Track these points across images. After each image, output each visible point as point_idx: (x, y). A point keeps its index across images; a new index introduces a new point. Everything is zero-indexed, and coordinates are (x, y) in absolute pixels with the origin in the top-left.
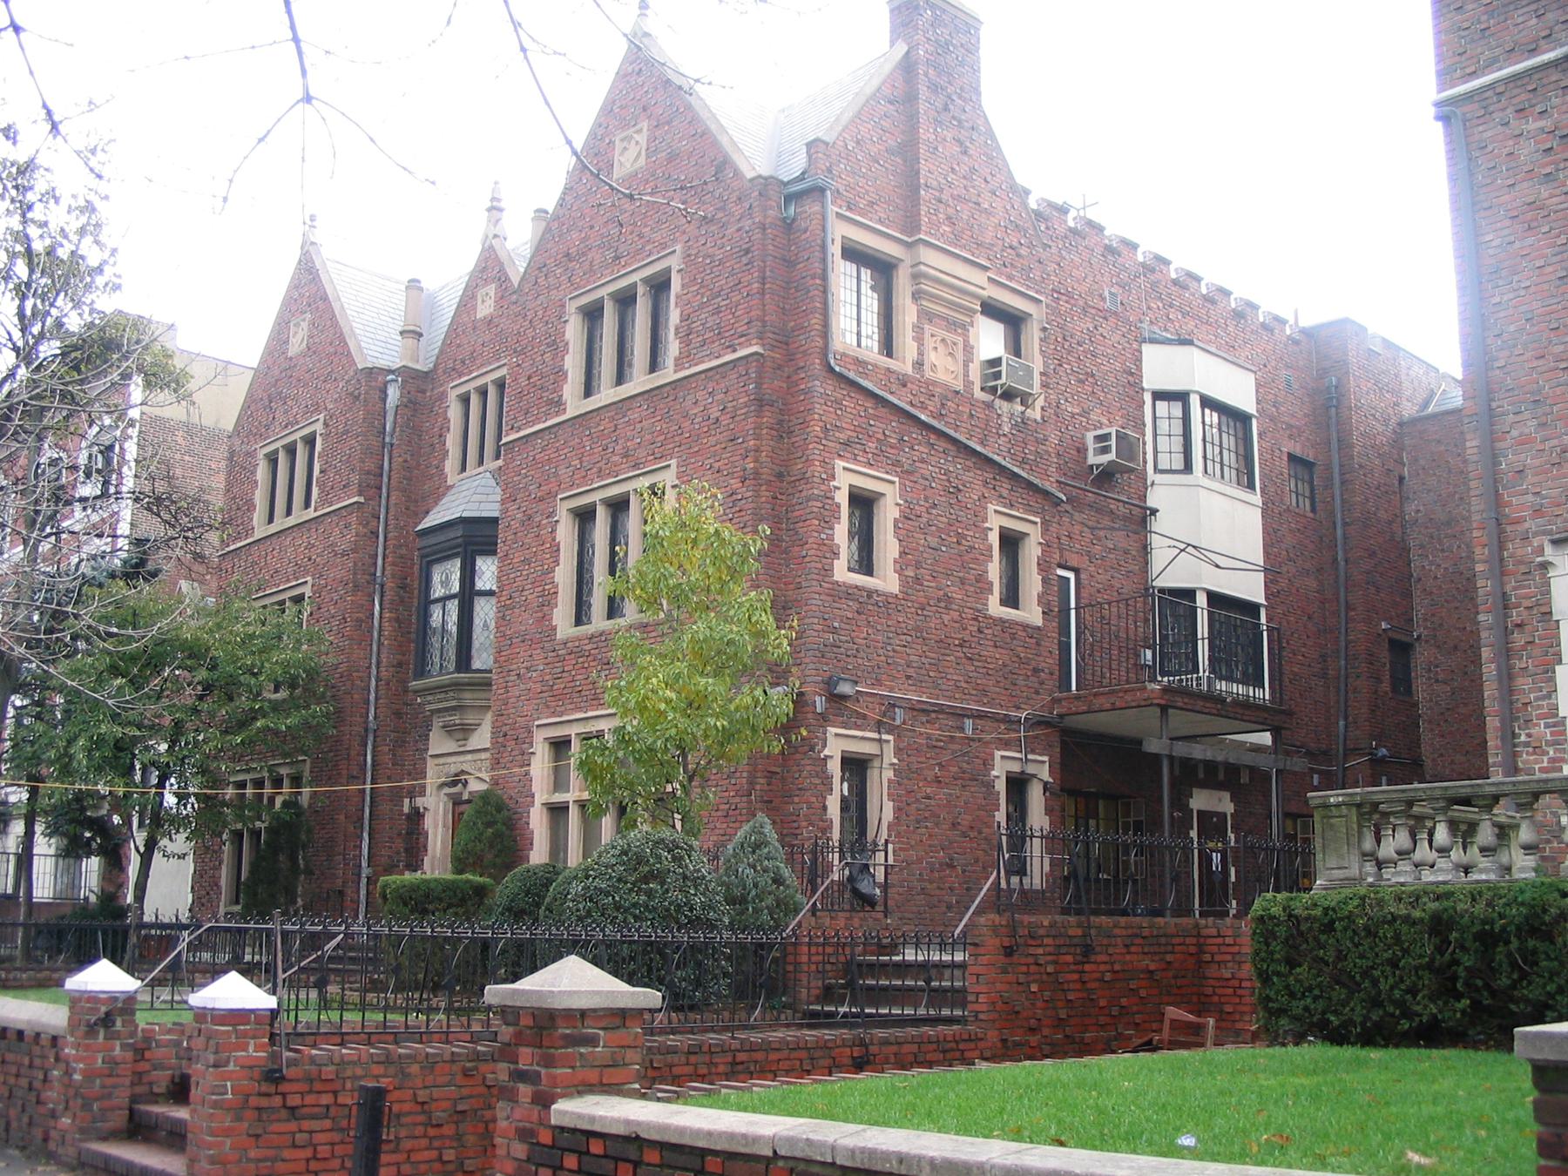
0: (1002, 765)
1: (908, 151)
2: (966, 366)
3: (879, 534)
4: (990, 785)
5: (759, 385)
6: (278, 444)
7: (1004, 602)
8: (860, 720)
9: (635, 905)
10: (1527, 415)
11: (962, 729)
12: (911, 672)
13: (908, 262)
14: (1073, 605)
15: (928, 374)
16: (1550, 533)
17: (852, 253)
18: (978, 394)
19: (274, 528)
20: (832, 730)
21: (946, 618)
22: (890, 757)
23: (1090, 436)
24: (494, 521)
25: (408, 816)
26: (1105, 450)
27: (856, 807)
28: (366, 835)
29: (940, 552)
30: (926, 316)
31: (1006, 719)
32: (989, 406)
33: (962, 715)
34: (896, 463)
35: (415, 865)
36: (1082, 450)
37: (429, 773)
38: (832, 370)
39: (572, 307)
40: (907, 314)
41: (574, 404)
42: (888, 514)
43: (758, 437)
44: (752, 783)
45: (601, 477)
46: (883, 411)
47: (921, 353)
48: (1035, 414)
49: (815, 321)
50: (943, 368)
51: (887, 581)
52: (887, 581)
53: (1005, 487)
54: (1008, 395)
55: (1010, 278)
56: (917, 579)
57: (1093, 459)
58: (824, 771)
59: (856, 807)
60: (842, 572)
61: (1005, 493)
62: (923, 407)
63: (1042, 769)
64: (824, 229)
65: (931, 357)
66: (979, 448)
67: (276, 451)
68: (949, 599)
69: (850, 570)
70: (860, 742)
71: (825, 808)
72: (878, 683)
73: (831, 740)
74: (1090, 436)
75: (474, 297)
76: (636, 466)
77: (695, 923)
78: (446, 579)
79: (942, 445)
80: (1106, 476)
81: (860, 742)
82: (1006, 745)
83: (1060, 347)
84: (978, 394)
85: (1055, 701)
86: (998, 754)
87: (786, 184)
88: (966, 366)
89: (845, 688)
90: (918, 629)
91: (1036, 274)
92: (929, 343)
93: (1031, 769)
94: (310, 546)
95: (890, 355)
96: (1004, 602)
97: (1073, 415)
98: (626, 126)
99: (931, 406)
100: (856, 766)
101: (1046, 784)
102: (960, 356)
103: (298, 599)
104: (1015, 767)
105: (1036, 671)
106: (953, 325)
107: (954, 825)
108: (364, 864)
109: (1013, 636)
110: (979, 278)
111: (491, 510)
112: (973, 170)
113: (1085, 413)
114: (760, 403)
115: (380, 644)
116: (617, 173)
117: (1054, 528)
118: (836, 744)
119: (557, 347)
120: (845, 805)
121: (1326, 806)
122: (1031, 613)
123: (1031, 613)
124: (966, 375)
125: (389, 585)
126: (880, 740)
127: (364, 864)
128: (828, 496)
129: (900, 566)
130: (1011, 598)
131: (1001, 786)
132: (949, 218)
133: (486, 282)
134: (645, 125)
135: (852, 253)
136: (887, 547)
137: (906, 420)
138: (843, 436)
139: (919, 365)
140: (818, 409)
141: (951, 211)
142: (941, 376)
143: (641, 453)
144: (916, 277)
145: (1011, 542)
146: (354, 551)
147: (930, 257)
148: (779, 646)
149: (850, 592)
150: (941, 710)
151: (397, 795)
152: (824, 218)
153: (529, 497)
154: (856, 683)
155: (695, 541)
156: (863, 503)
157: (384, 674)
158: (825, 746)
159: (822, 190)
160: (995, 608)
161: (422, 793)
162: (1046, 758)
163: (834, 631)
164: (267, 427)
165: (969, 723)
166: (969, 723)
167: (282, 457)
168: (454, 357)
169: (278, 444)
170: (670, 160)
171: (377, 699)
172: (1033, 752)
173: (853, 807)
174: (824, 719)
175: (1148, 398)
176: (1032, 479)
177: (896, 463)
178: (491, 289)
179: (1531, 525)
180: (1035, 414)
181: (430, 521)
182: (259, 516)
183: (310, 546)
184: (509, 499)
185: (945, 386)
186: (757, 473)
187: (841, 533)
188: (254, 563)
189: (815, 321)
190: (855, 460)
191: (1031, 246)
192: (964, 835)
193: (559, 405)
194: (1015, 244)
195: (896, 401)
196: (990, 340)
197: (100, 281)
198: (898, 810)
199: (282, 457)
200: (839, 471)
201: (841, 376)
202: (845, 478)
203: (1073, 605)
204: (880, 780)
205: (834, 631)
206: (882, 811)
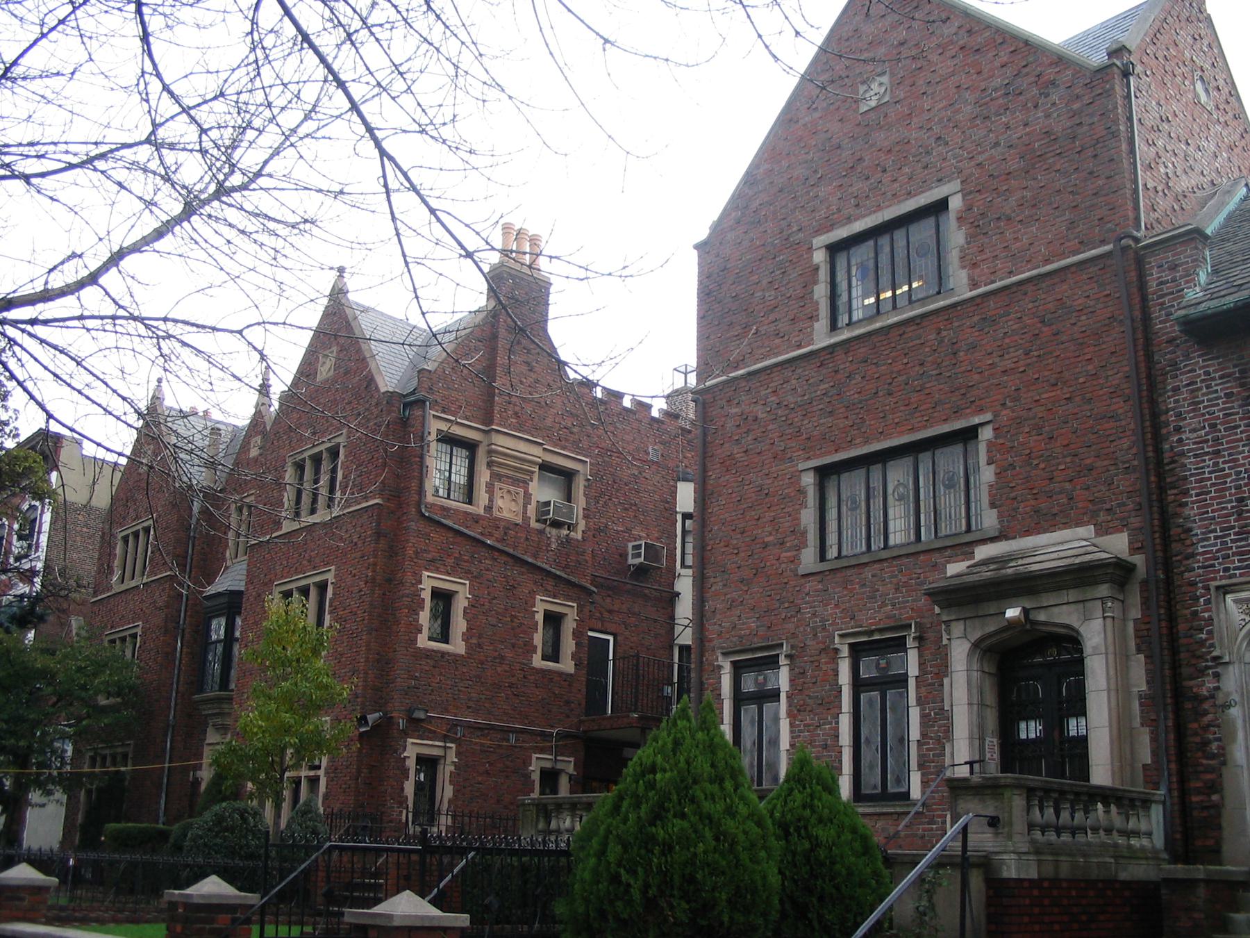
0: (537, 763)
1: (490, 369)
2: (525, 507)
3: (446, 616)
4: (527, 776)
5: (378, 524)
6: (129, 531)
7: (545, 657)
8: (433, 735)
9: (216, 845)
10: (719, 579)
11: (508, 740)
12: (471, 704)
13: (485, 443)
14: (611, 657)
15: (496, 513)
16: (722, 648)
17: (449, 440)
18: (534, 524)
19: (123, 587)
20: (410, 740)
21: (499, 669)
22: (452, 757)
23: (630, 545)
24: (241, 593)
25: (192, 783)
26: (639, 555)
27: (427, 790)
28: (163, 795)
29: (499, 628)
30: (495, 476)
31: (542, 734)
32: (542, 532)
33: (507, 731)
34: (469, 572)
35: (556, 793)
36: (624, 556)
37: (205, 755)
38: (423, 515)
39: (289, 462)
40: (483, 476)
41: (287, 527)
42: (460, 603)
43: (375, 556)
44: (359, 771)
45: (297, 573)
46: (459, 539)
47: (491, 500)
48: (578, 535)
49: (414, 484)
50: (507, 508)
51: (457, 646)
52: (457, 646)
53: (550, 585)
54: (556, 524)
55: (564, 448)
56: (479, 645)
57: (631, 561)
58: (404, 766)
59: (427, 790)
60: (423, 641)
61: (550, 588)
62: (491, 535)
63: (568, 765)
64: (423, 426)
65: (500, 502)
66: (530, 560)
67: (127, 536)
68: (502, 658)
69: (430, 639)
70: (431, 747)
71: (402, 789)
72: (446, 711)
73: (409, 747)
74: (630, 545)
75: (249, 443)
76: (314, 568)
77: (251, 856)
78: (218, 628)
79: (504, 558)
80: (641, 571)
81: (431, 747)
82: (542, 751)
83: (601, 491)
84: (534, 524)
85: (581, 722)
86: (535, 756)
87: (405, 396)
88: (525, 507)
89: (420, 715)
90: (479, 677)
91: (585, 443)
92: (498, 494)
93: (559, 766)
94: (142, 601)
95: (470, 503)
96: (545, 657)
97: (618, 532)
98: (325, 349)
99: (497, 534)
100: (428, 764)
101: (571, 776)
102: (521, 501)
103: (134, 636)
104: (548, 765)
105: (568, 703)
106: (516, 482)
107: (498, 802)
108: (161, 815)
109: (551, 680)
110: (536, 451)
111: (241, 586)
112: (537, 381)
113: (628, 530)
114: (379, 535)
115: (179, 669)
116: (319, 378)
117: (586, 610)
118: (412, 749)
119: (280, 485)
120: (419, 786)
121: (524, 805)
122: (567, 665)
123: (567, 665)
124: (525, 512)
125: (187, 631)
126: (445, 747)
127: (161, 815)
128: (417, 594)
129: (466, 637)
130: (553, 654)
131: (536, 777)
132: (516, 413)
133: (257, 434)
134: (335, 349)
135: (449, 440)
136: (459, 624)
137: (473, 543)
138: (430, 556)
139: (489, 508)
140: (413, 540)
141: (517, 409)
142: (506, 515)
143: (317, 560)
144: (490, 452)
145: (553, 620)
146: (167, 607)
147: (501, 442)
148: (341, 695)
149: (429, 654)
150: (492, 727)
151: (186, 770)
152: (424, 417)
153: (260, 580)
154: (427, 711)
155: (293, 631)
156: (443, 598)
157: (181, 689)
158: (405, 749)
159: (424, 402)
160: (537, 661)
161: (200, 769)
162: (572, 759)
163: (415, 678)
164: (124, 518)
165: (512, 737)
166: (512, 737)
167: (131, 539)
168: (235, 483)
169: (129, 531)
170: (345, 374)
171: (176, 704)
172: (562, 755)
173: (427, 788)
174: (405, 734)
175: (679, 518)
176: (571, 578)
177: (469, 572)
178: (258, 439)
179: (716, 643)
180: (578, 535)
181: (211, 590)
182: (822, 324)
183: (142, 601)
184: (249, 582)
185: (508, 521)
186: (374, 579)
187: (424, 617)
188: (111, 610)
189: (414, 484)
190: (437, 570)
191: (581, 426)
192: (506, 807)
193: (109, 588)
194: (569, 425)
195: (472, 534)
196: (544, 492)
197: (7, 430)
198: (456, 792)
199: (131, 539)
200: (424, 579)
201: (430, 519)
202: (429, 582)
203: (611, 657)
204: (446, 770)
205: (415, 678)
206: (446, 791)
